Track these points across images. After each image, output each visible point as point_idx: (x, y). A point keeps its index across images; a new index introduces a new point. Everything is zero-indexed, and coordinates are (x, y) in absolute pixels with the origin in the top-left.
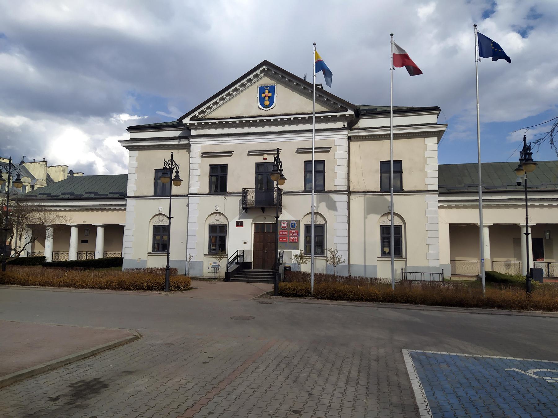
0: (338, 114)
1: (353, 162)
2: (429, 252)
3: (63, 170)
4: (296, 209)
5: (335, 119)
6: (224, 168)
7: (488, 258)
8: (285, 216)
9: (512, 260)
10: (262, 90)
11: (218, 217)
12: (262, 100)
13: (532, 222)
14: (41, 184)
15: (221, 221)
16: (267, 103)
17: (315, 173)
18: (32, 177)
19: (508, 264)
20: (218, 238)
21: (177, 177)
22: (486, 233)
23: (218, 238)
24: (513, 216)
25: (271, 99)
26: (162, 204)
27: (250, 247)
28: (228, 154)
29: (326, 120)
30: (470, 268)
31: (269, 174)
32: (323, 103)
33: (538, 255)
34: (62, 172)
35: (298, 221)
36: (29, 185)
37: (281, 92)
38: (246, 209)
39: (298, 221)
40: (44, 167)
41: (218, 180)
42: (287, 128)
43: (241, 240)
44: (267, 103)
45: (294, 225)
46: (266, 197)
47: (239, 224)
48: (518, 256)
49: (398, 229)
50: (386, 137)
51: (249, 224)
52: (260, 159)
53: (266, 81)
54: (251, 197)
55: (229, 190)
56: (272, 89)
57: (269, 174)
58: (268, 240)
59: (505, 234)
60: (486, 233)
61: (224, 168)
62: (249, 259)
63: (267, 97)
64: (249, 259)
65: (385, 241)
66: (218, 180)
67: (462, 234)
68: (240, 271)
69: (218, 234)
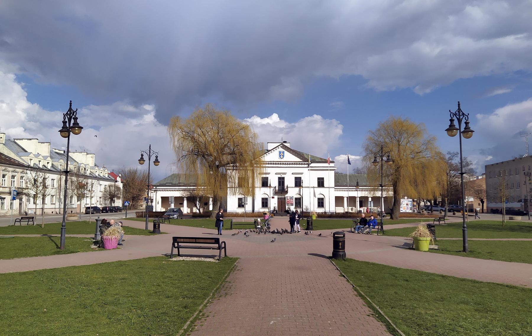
1: (310, 177)
2: (330, 207)
4: (293, 193)
5: (304, 164)
6: (283, 178)
7: (345, 208)
10: (280, 152)
12: (280, 156)
13: (384, 196)
15: (266, 196)
16: (282, 157)
17: (298, 183)
19: (352, 209)
20: (265, 203)
22: (345, 199)
23: (265, 203)
24: (378, 194)
25: (283, 156)
26: (321, 190)
27: (276, 205)
28: (285, 174)
29: (302, 164)
31: (281, 181)
33: (361, 206)
38: (276, 193)
43: (274, 203)
44: (282, 157)
45: (292, 198)
46: (282, 189)
47: (273, 198)
49: (322, 199)
50: (328, 170)
51: (276, 197)
52: (280, 176)
53: (281, 149)
54: (277, 188)
55: (325, 186)
56: (283, 152)
57: (281, 181)
58: (282, 202)
59: (352, 200)
60: (345, 199)
61: (283, 178)
62: (277, 209)
63: (281, 155)
64: (277, 209)
65: (319, 203)
66: (265, 183)
67: (339, 200)
68: (274, 213)
69: (265, 201)
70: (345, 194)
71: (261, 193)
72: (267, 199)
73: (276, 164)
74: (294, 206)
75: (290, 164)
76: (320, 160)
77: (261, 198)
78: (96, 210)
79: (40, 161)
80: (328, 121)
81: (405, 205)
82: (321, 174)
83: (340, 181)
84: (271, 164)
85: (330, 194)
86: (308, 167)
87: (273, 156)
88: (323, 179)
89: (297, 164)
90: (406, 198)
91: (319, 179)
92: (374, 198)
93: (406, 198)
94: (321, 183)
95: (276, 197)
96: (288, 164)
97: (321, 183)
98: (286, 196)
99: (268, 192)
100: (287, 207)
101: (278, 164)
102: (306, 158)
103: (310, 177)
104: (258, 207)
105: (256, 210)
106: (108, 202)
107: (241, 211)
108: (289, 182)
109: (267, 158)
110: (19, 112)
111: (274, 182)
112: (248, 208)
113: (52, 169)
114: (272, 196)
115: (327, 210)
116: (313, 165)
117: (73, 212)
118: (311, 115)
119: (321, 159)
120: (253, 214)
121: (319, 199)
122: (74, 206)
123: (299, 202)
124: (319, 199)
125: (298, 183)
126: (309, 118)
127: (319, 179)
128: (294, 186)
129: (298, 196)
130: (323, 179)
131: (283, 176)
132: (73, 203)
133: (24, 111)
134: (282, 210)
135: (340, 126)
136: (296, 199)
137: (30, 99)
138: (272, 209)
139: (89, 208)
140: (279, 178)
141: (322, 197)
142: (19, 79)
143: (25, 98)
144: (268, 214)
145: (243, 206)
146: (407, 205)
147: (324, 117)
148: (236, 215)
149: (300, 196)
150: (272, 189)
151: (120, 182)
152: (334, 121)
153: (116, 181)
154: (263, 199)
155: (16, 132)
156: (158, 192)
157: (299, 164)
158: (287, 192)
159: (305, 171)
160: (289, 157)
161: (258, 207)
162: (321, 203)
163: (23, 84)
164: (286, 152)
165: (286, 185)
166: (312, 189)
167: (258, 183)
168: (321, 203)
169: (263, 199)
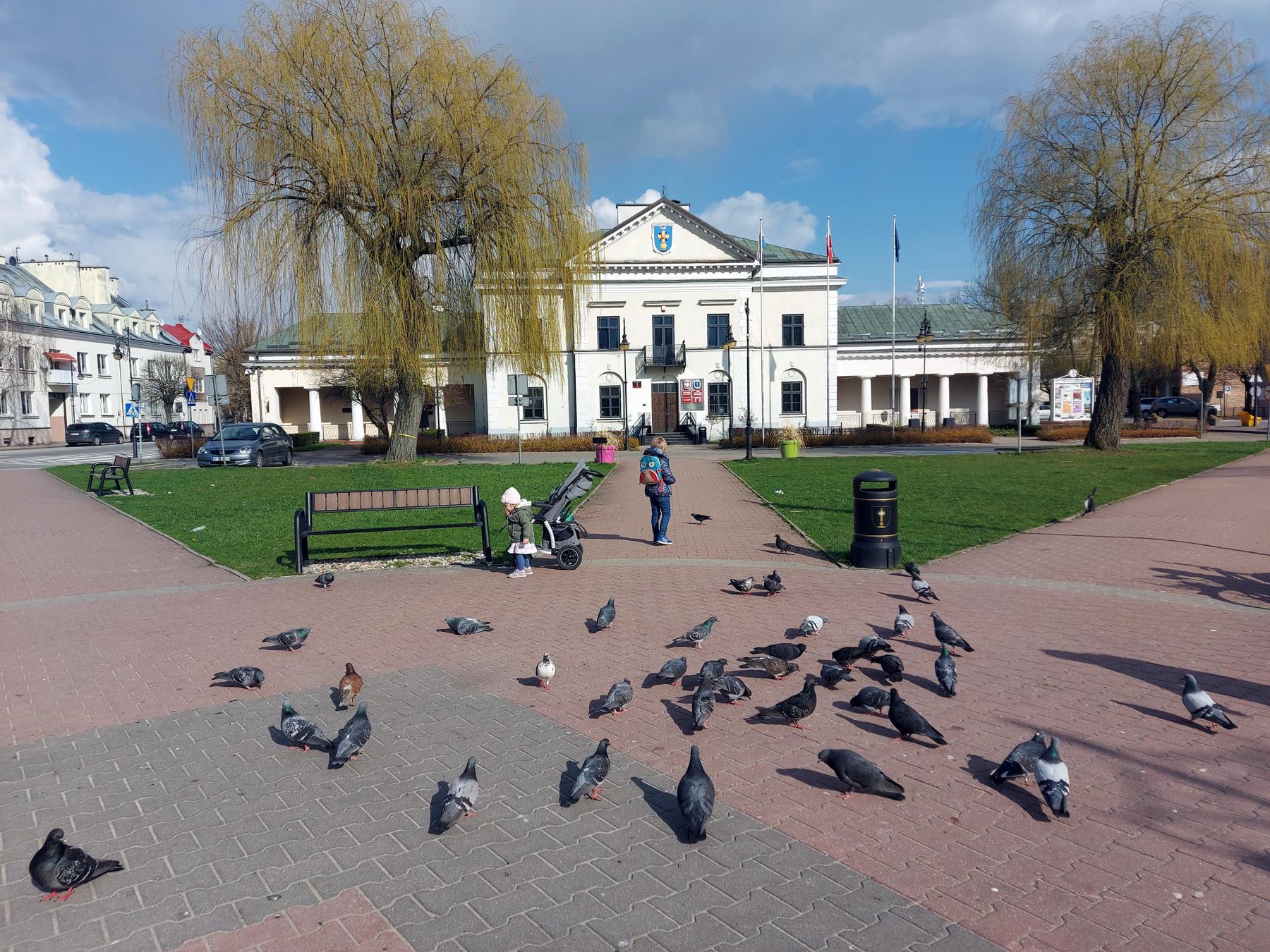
0: (745, 264)
2: (821, 410)
3: (99, 277)
4: (701, 367)
5: (740, 269)
6: (670, 319)
8: (687, 376)
9: (889, 411)
10: (657, 230)
11: (609, 376)
12: (658, 242)
14: (1087, 418)
15: (616, 382)
16: (664, 246)
17: (719, 333)
18: (47, 290)
20: (611, 402)
21: (625, 340)
23: (611, 402)
25: (669, 242)
26: (793, 356)
27: (648, 410)
28: (675, 303)
29: (732, 269)
30: (850, 420)
31: (663, 329)
32: (727, 251)
34: (98, 281)
35: (702, 380)
36: (67, 309)
37: (679, 233)
38: (646, 370)
39: (702, 380)
40: (74, 272)
41: (610, 336)
42: (687, 276)
43: (639, 404)
44: (664, 246)
45: (698, 384)
46: (665, 356)
47: (637, 385)
48: (898, 408)
49: (797, 386)
51: (647, 383)
53: (661, 219)
54: (650, 354)
55: (807, 341)
56: (669, 230)
57: (663, 329)
58: (666, 400)
59: (885, 387)
61: (670, 319)
62: (649, 421)
63: (662, 239)
64: (649, 421)
65: (785, 398)
66: (610, 336)
67: (848, 388)
68: (642, 435)
70: (868, 368)
71: (596, 370)
72: (616, 390)
73: (644, 270)
74: (706, 412)
75: (691, 270)
76: (792, 257)
77: (584, 386)
78: (104, 434)
79: (135, 324)
80: (781, 206)
81: (1070, 398)
82: (793, 303)
83: (856, 329)
84: (628, 270)
85: (820, 368)
86: (751, 279)
87: (635, 244)
88: (799, 318)
89: (715, 269)
90: (1073, 373)
91: (787, 319)
92: (957, 380)
93: (1073, 373)
94: (793, 332)
95: (647, 383)
96: (684, 270)
97: (793, 332)
98: (680, 377)
99: (622, 366)
100: (682, 414)
101: (652, 270)
102: (743, 250)
103: (758, 319)
104: (590, 418)
105: (582, 426)
106: (161, 410)
107: (533, 429)
108: (690, 331)
109: (613, 251)
110: (35, 200)
111: (639, 333)
112: (557, 420)
113: (94, 330)
114: (632, 378)
115: (812, 423)
116: (766, 272)
117: (38, 440)
118: (738, 193)
119: (793, 252)
120: (574, 441)
121: (786, 386)
122: (39, 423)
123: (720, 398)
124: (786, 386)
125: (719, 333)
126: (733, 202)
127: (787, 319)
128: (705, 344)
129: (720, 379)
130: (799, 318)
131: (669, 311)
132: (34, 412)
133: (48, 195)
134: (668, 421)
135: (810, 219)
136: (712, 387)
137: (60, 164)
138: (633, 421)
139: (80, 427)
140: (657, 320)
141: (796, 378)
142: (22, 113)
143: (46, 164)
144: (613, 442)
145: (616, 413)
146: (1077, 396)
147: (771, 197)
148: (511, 445)
149: (726, 379)
150: (632, 357)
151: (202, 352)
152: (796, 208)
153: (189, 350)
154: (604, 390)
155: (30, 246)
156: (266, 373)
157: (723, 269)
158: (682, 366)
159: (742, 292)
160: (687, 245)
161: (590, 418)
162: (793, 398)
163: (32, 126)
164: (678, 230)
165: (678, 342)
166: (766, 354)
167: (588, 336)
168: (793, 398)
169: (604, 390)
